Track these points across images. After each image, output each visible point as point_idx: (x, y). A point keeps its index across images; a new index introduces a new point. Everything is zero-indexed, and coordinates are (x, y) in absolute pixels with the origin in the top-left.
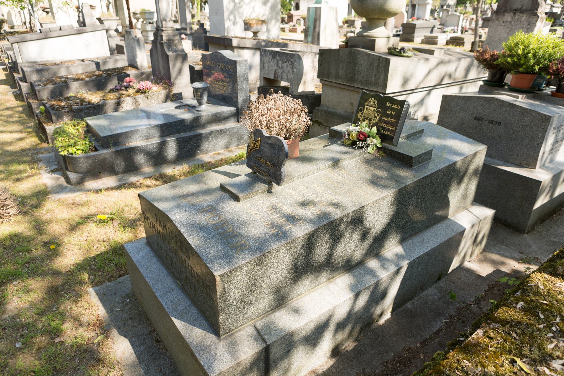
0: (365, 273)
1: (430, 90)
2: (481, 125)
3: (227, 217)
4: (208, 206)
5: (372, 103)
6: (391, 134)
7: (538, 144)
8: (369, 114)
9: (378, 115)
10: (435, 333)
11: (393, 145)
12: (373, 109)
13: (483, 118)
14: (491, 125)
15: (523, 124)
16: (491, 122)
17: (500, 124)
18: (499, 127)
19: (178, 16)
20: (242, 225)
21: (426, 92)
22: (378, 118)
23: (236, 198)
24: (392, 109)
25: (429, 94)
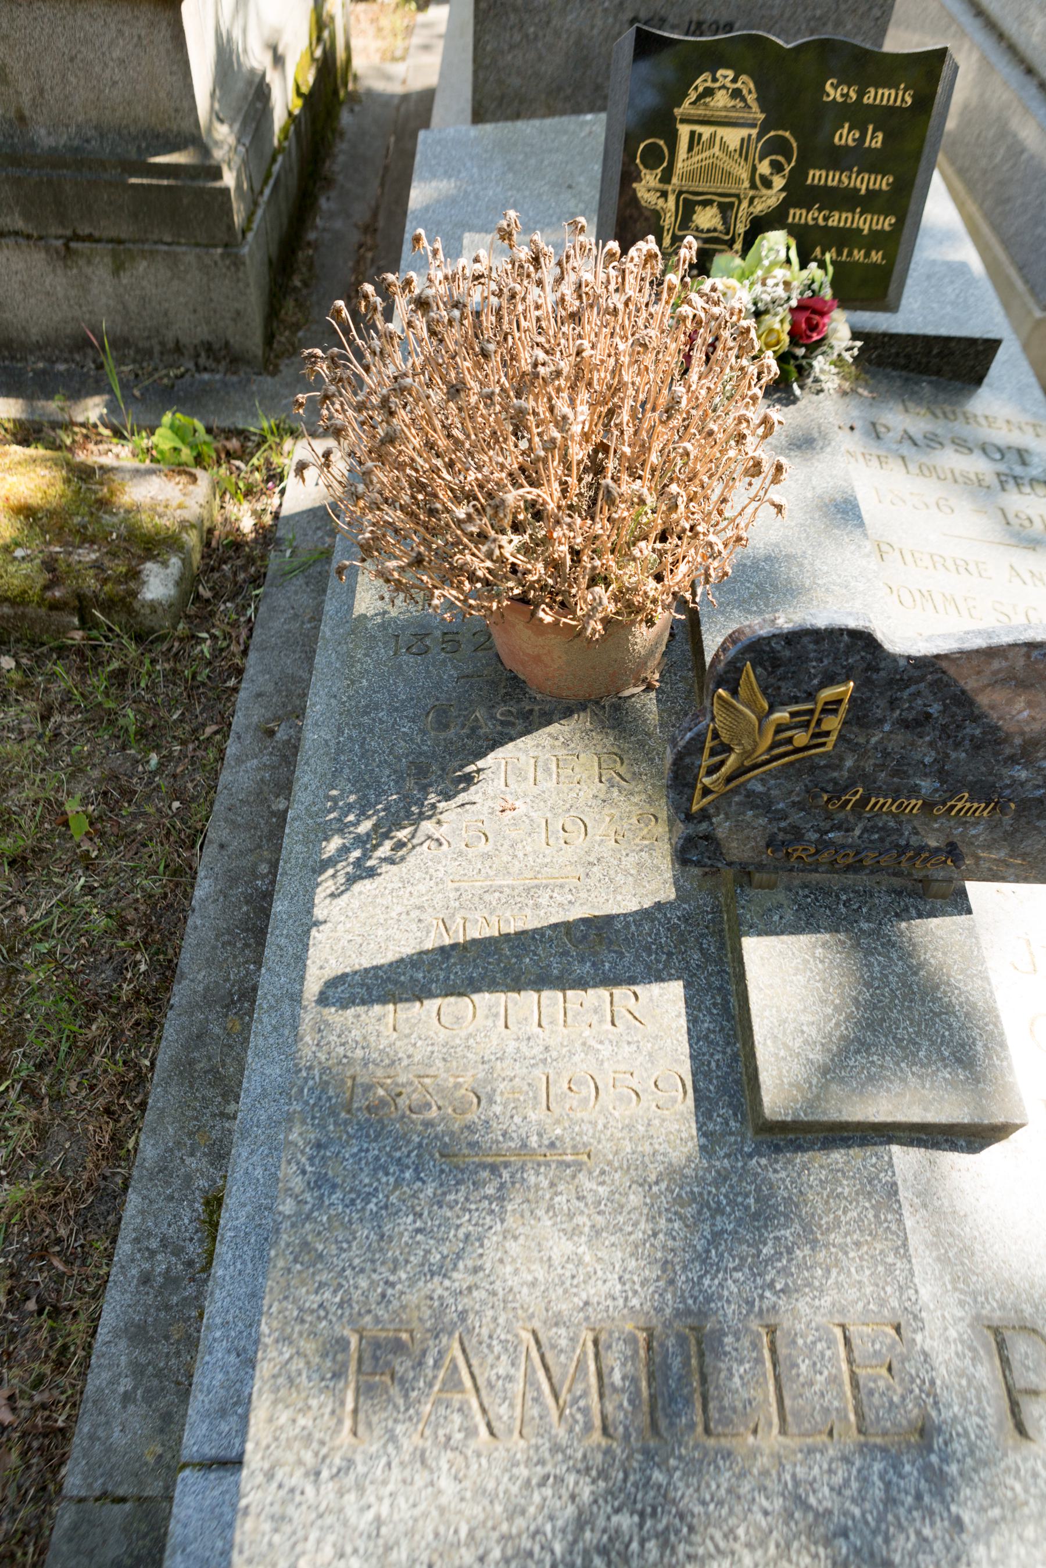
6: (876, 257)
9: (777, 167)
12: (733, 137)
22: (779, 182)
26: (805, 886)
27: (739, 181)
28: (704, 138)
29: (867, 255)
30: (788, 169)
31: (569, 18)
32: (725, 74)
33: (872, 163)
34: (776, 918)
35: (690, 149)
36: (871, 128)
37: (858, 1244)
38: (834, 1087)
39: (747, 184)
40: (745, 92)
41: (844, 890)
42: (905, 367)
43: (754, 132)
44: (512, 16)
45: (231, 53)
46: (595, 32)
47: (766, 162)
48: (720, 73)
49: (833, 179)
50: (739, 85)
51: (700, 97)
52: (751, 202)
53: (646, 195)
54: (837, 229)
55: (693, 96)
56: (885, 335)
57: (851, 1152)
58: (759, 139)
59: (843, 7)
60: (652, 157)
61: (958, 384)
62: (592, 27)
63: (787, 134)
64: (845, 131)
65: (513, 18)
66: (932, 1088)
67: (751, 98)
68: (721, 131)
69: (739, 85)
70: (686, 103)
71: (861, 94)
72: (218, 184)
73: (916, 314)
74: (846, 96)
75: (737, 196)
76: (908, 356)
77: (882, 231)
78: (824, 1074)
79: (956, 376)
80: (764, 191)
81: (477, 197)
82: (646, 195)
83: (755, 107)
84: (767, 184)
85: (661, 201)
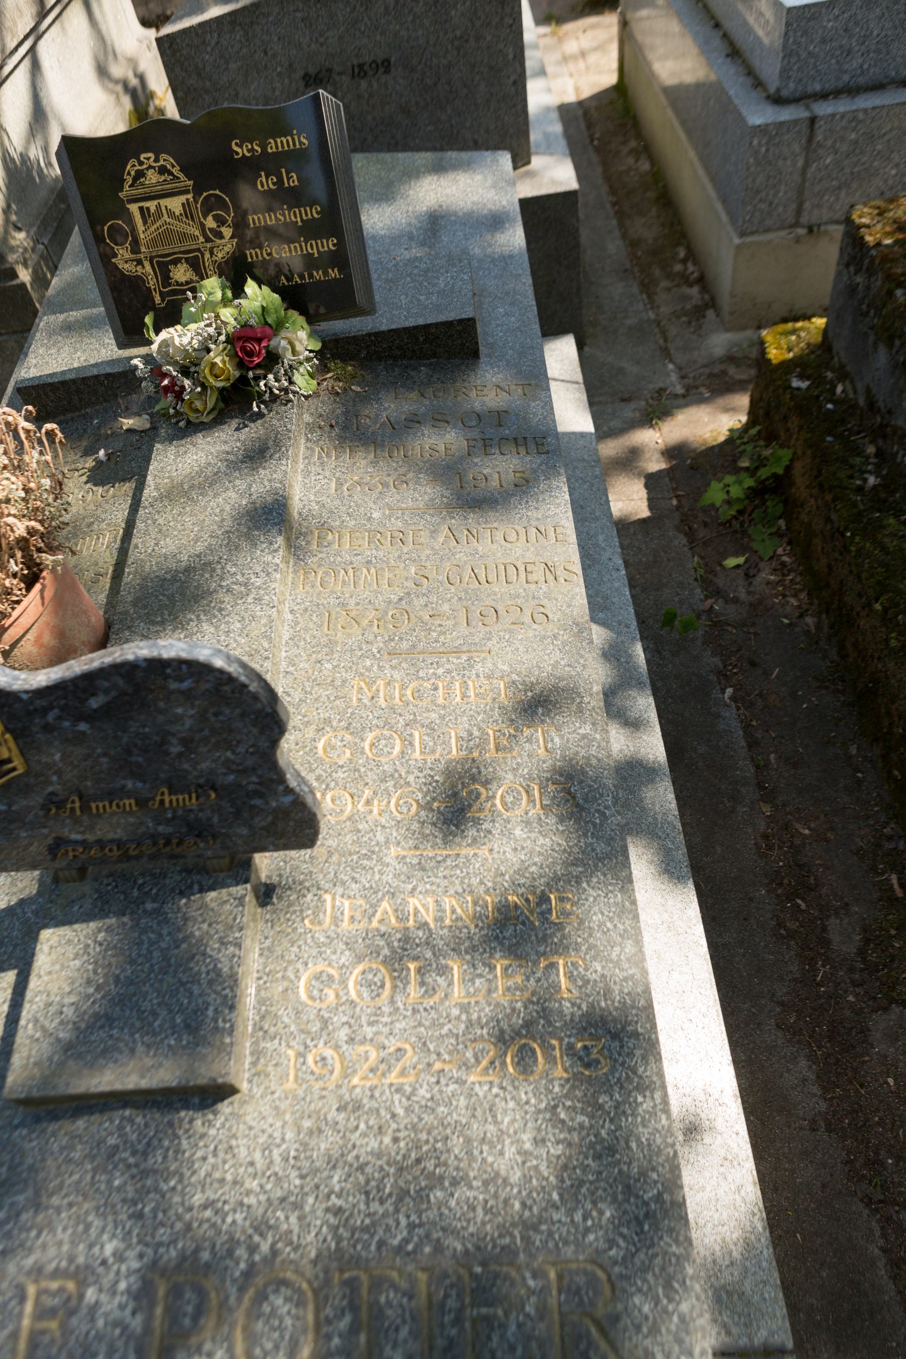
0: (632, 792)
1: (32, 50)
3: (307, 1234)
4: (143, 1295)
5: (152, 177)
6: (334, 273)
8: (167, 235)
9: (221, 221)
10: (750, 747)
11: (363, 312)
12: (175, 204)
13: (330, 71)
14: (364, 84)
17: (386, 65)
20: (422, 1196)
21: (27, 63)
22: (227, 232)
23: (217, 1093)
25: (36, 67)
26: (111, 875)
27: (195, 238)
29: (326, 273)
31: (252, 88)
34: (76, 908)
35: (145, 222)
37: (70, 1205)
38: (71, 1063)
39: (202, 239)
40: (169, 167)
41: (143, 874)
43: (190, 196)
44: (206, 97)
45: (29, 171)
47: (210, 218)
48: (142, 156)
50: (162, 162)
51: (135, 179)
52: (212, 253)
53: (126, 266)
55: (129, 180)
56: (369, 335)
57: (93, 1118)
58: (196, 202)
59: (478, 23)
61: (457, 361)
62: (274, 90)
63: (217, 192)
64: (264, 180)
66: (155, 1055)
67: (176, 171)
68: (164, 202)
70: (126, 187)
72: (15, 282)
74: (252, 150)
75: (198, 250)
77: (330, 251)
78: (66, 1051)
80: (218, 241)
82: (126, 266)
83: (181, 176)
84: (220, 236)
85: (139, 268)
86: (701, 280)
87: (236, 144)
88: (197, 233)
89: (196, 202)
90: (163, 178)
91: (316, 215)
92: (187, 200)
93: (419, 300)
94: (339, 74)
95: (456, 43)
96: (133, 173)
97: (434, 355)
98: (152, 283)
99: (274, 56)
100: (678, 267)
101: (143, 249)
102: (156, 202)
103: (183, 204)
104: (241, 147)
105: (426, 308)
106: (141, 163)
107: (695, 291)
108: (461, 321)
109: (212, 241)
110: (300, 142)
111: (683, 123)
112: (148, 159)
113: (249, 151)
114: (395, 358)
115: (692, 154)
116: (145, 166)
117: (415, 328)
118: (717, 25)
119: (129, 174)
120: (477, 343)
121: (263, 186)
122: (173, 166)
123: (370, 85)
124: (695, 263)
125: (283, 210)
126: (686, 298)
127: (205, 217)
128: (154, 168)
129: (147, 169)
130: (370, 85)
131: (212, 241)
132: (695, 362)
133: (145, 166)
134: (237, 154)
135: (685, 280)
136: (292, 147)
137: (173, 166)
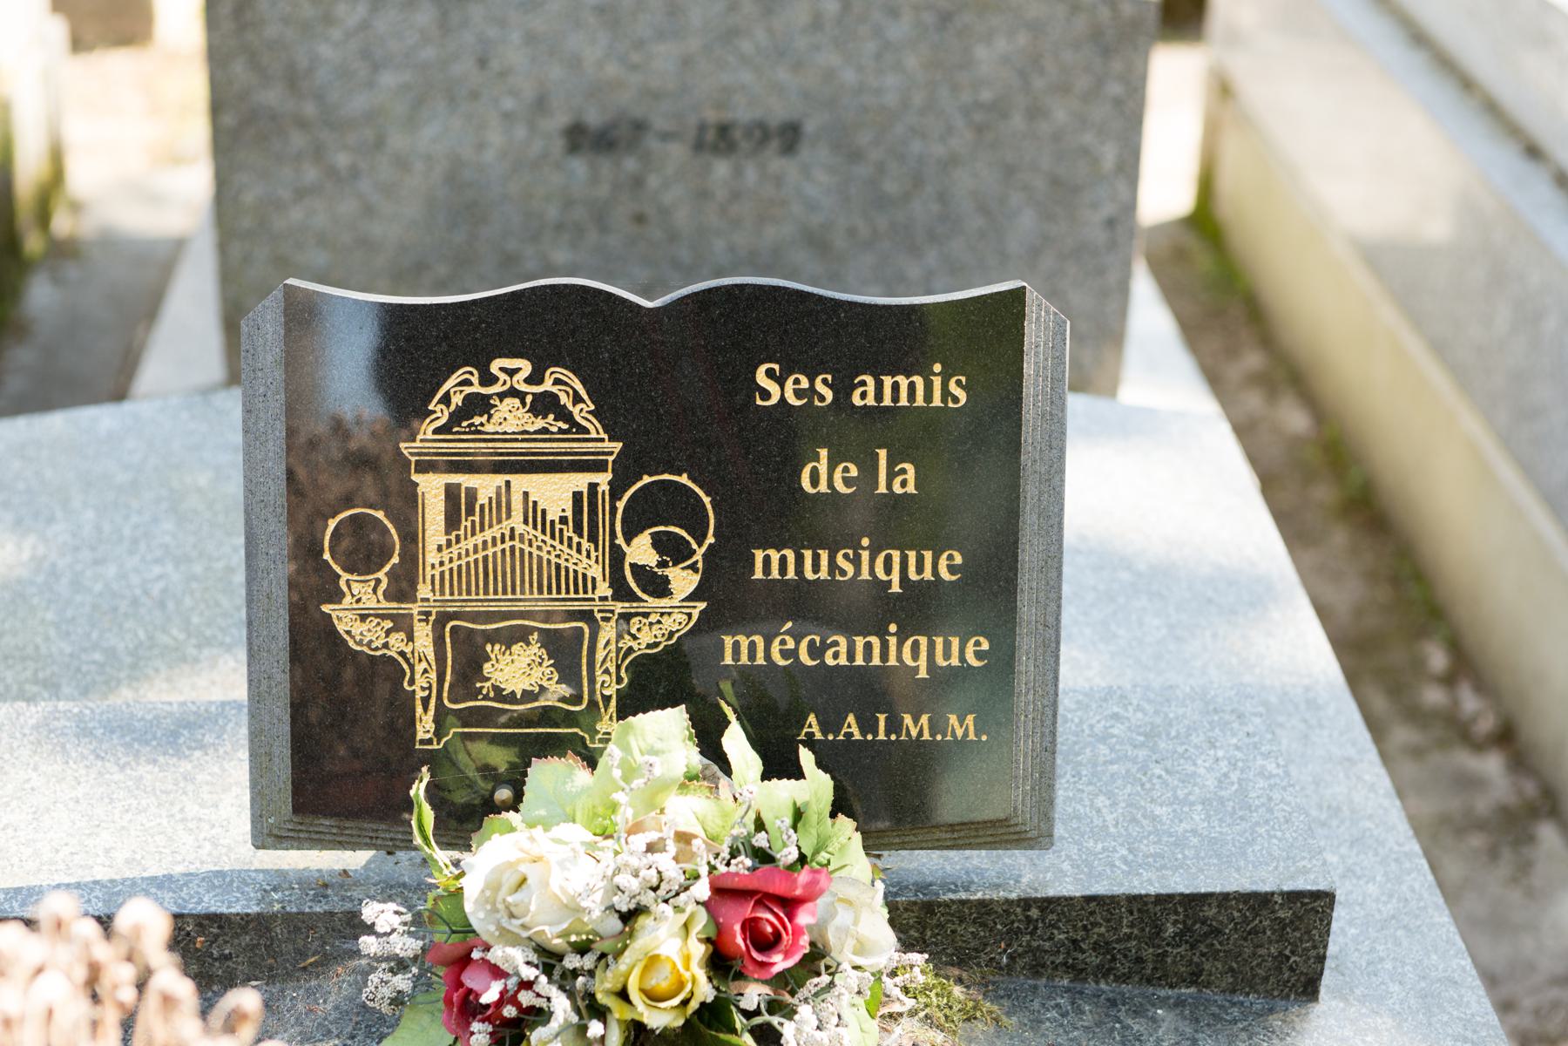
2: (638, 182)
5: (510, 418)
7: (1111, 223)
9: (672, 550)
12: (555, 493)
13: (640, 127)
14: (721, 169)
15: (966, 97)
16: (720, 139)
17: (790, 136)
18: (787, 167)
19: (569, 514)
22: (683, 580)
24: (859, 432)
27: (587, 583)
28: (482, 499)
30: (700, 552)
32: (514, 369)
33: (895, 523)
35: (452, 522)
36: (883, 454)
39: (604, 589)
40: (564, 399)
42: (1104, 972)
43: (603, 480)
46: (489, 156)
47: (644, 540)
49: (816, 567)
50: (548, 386)
51: (457, 417)
53: (358, 628)
54: (850, 672)
55: (442, 415)
58: (615, 494)
59: (1039, 83)
60: (364, 551)
61: (1256, 1001)
64: (823, 467)
65: (298, 140)
68: (520, 482)
69: (548, 386)
70: (427, 429)
71: (843, 389)
73: (1098, 846)
75: (587, 616)
76: (1100, 946)
79: (1243, 982)
80: (652, 602)
81: (77, 585)
82: (358, 628)
83: (595, 428)
84: (659, 587)
85: (397, 641)
86: (1506, 737)
87: (770, 374)
88: (595, 571)
89: (615, 494)
90: (540, 423)
91: (945, 575)
92: (593, 487)
93: (1154, 819)
94: (666, 136)
95: (978, 117)
96: (457, 400)
97: (1194, 978)
98: (421, 681)
99: (503, 74)
100: (1434, 696)
101: (424, 591)
102: (500, 479)
103: (577, 496)
104: (781, 383)
105: (1180, 843)
106: (488, 379)
107: (1492, 765)
108: (1293, 897)
109: (632, 597)
110: (946, 393)
111: (1439, 349)
112: (512, 373)
113: (798, 394)
114: (1078, 972)
115: (1471, 424)
116: (497, 388)
117: (1162, 900)
118: (1533, 152)
119: (446, 399)
120: (1321, 959)
121: (815, 481)
122: (577, 399)
123: (738, 172)
124: (1482, 687)
125: (857, 547)
126: (1469, 783)
127: (629, 537)
128: (521, 396)
129: (502, 396)
130: (738, 172)
131: (632, 597)
132: (1531, 967)
133: (497, 388)
134: (766, 395)
135: (1460, 732)
136: (920, 401)
137: (577, 399)
